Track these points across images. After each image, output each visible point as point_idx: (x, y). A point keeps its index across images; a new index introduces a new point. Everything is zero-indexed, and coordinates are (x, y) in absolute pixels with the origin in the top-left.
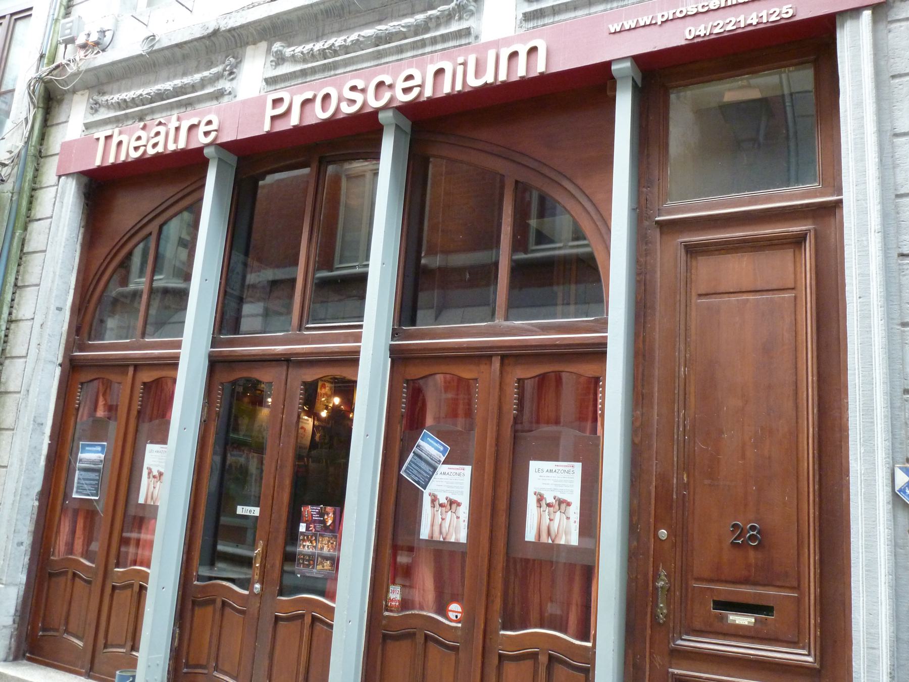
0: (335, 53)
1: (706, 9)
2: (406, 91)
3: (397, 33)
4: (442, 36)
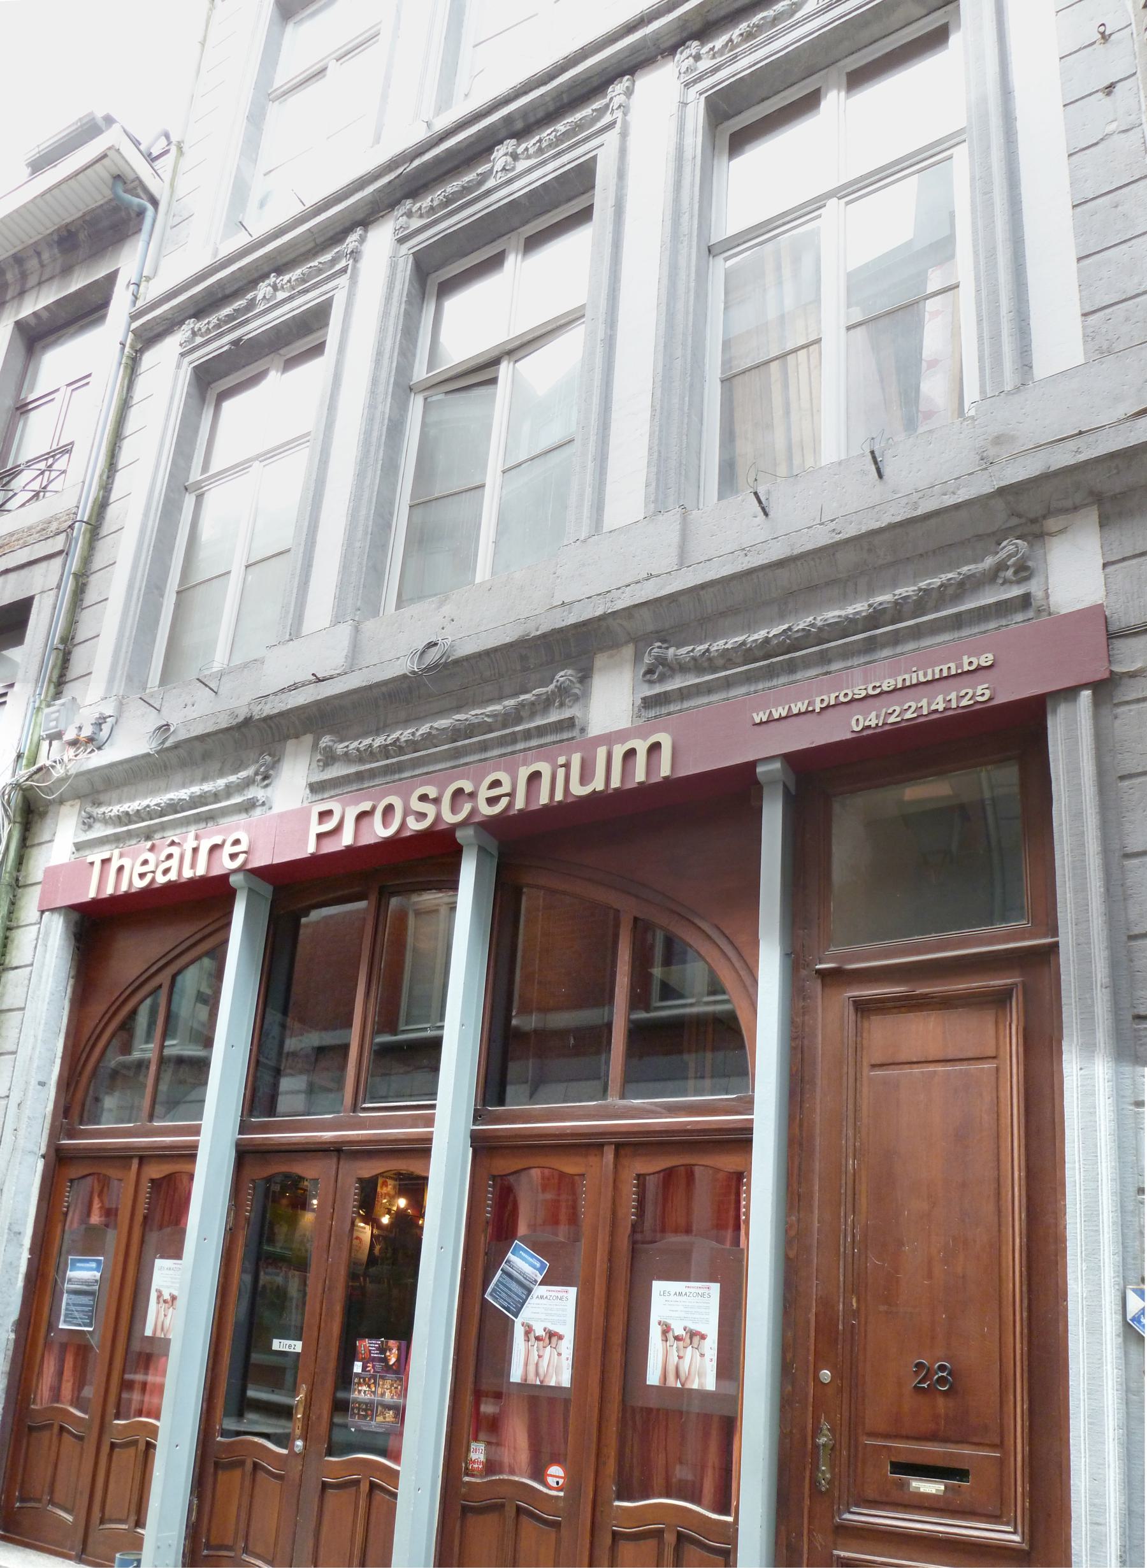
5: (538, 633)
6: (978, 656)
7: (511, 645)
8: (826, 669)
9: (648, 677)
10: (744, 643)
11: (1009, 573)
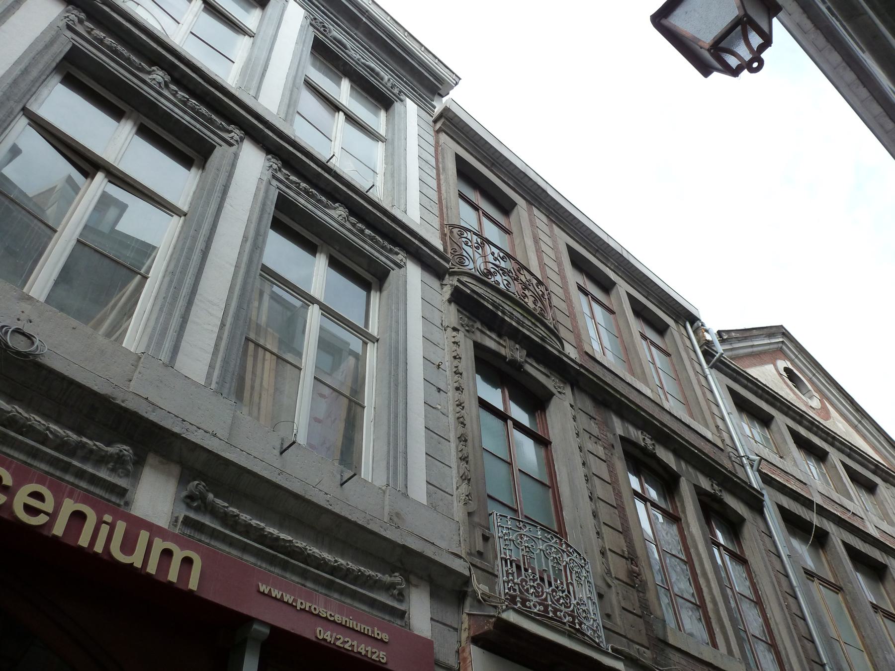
0: (44, 440)
1: (332, 619)
2: (29, 509)
3: (39, 432)
4: (93, 475)
5: (123, 405)
6: (383, 632)
7: (95, 394)
8: (303, 582)
9: (188, 501)
10: (263, 529)
11: (396, 592)
